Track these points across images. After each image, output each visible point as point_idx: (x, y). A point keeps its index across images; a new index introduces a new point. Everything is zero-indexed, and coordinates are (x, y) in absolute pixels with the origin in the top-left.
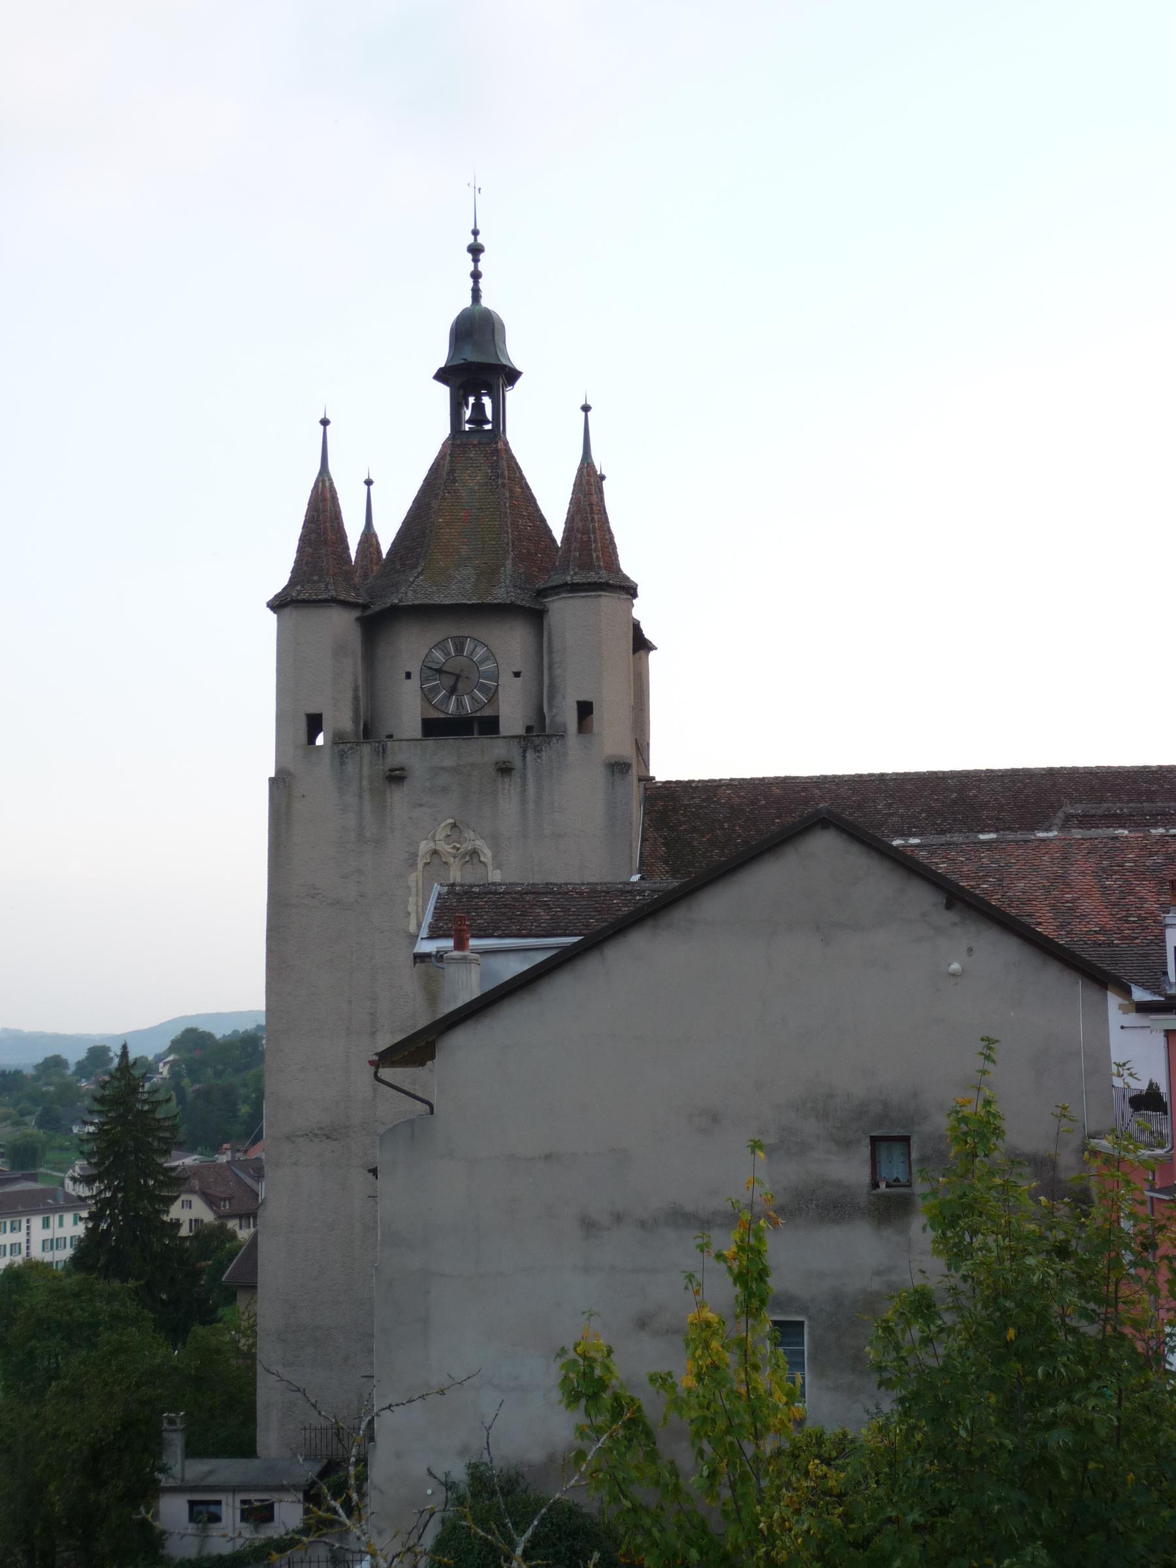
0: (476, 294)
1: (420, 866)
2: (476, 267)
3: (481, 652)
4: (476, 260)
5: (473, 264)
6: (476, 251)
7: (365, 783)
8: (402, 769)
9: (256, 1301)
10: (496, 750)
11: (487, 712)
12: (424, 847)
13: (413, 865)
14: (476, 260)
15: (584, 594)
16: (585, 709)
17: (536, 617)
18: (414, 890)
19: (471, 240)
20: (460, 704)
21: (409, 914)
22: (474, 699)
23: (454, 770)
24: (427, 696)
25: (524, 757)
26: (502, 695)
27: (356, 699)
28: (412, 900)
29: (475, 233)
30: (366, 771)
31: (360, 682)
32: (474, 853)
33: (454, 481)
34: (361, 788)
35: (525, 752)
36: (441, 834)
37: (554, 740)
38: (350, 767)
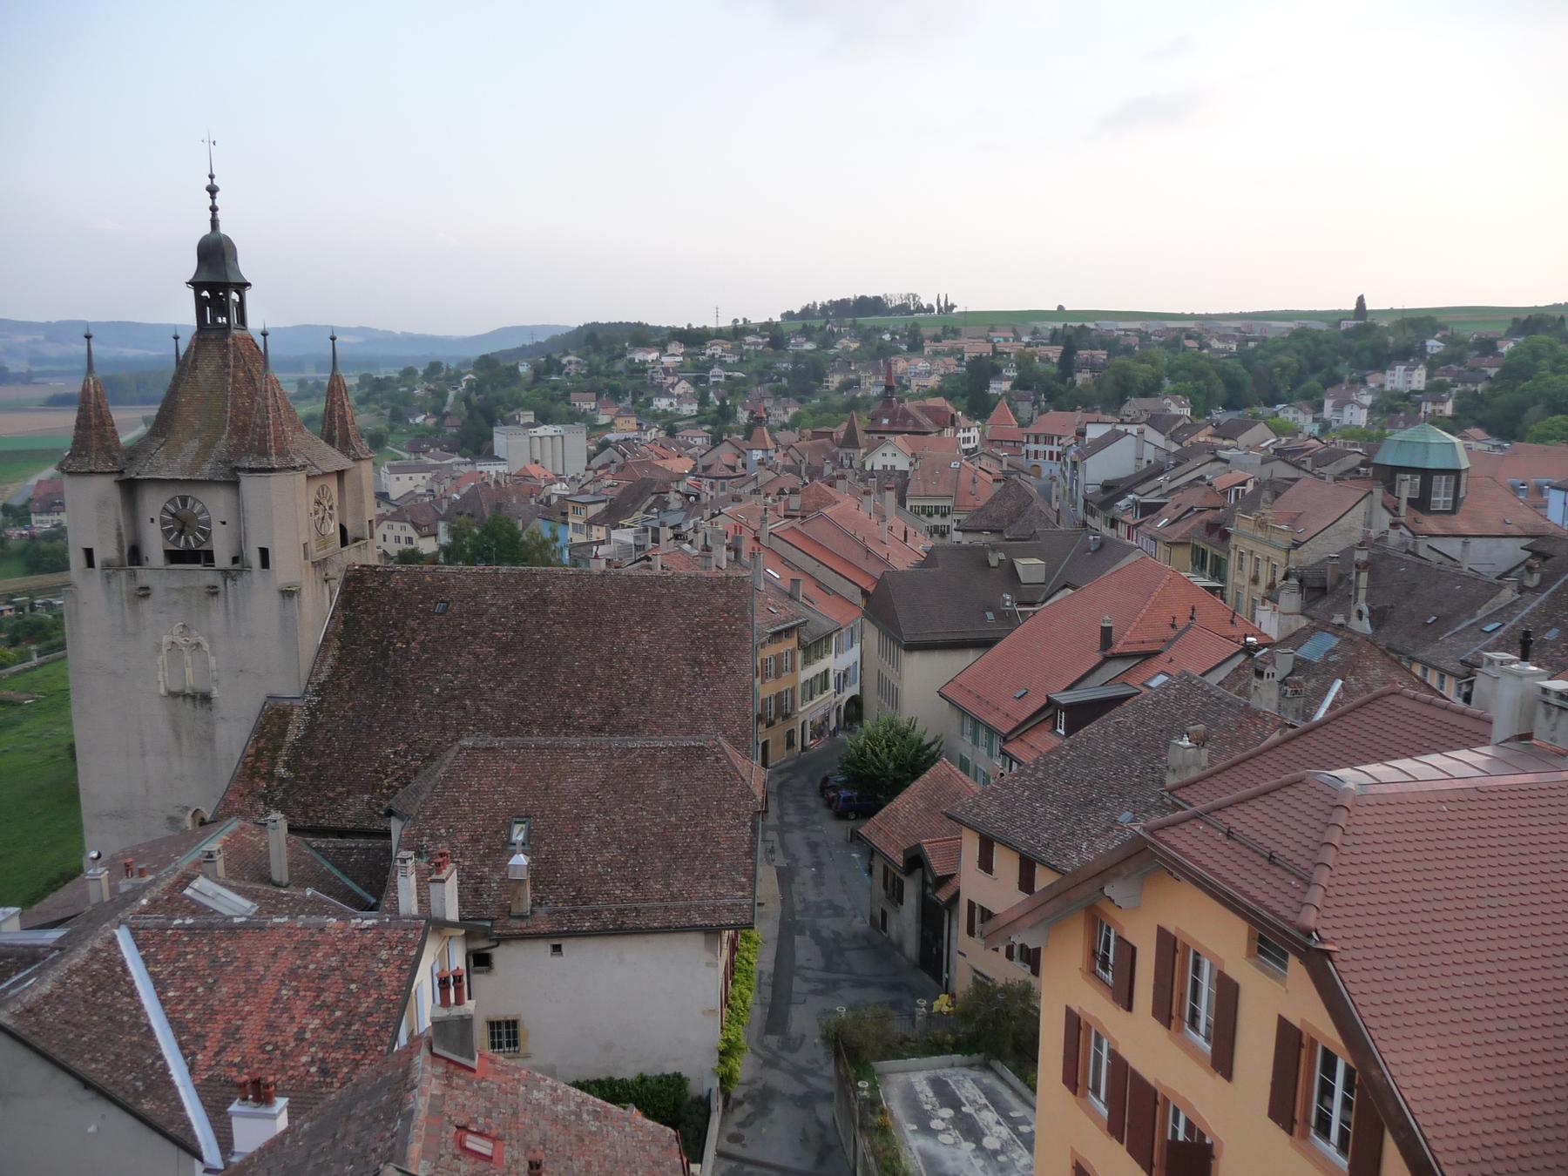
0: (214, 223)
1: (164, 651)
2: (213, 203)
3: (198, 508)
4: (213, 198)
6: (212, 191)
7: (124, 595)
8: (147, 588)
10: (208, 577)
11: (205, 547)
12: (166, 639)
13: (159, 651)
14: (213, 198)
16: (264, 553)
17: (235, 484)
18: (161, 667)
19: (208, 182)
20: (187, 541)
21: (159, 682)
22: (195, 538)
23: (181, 590)
24: (167, 533)
25: (225, 584)
26: (214, 536)
27: (119, 535)
28: (160, 673)
29: (212, 177)
30: (124, 588)
31: (122, 523)
32: (198, 644)
33: (196, 368)
35: (225, 580)
36: (177, 631)
37: (244, 573)
38: (114, 585)
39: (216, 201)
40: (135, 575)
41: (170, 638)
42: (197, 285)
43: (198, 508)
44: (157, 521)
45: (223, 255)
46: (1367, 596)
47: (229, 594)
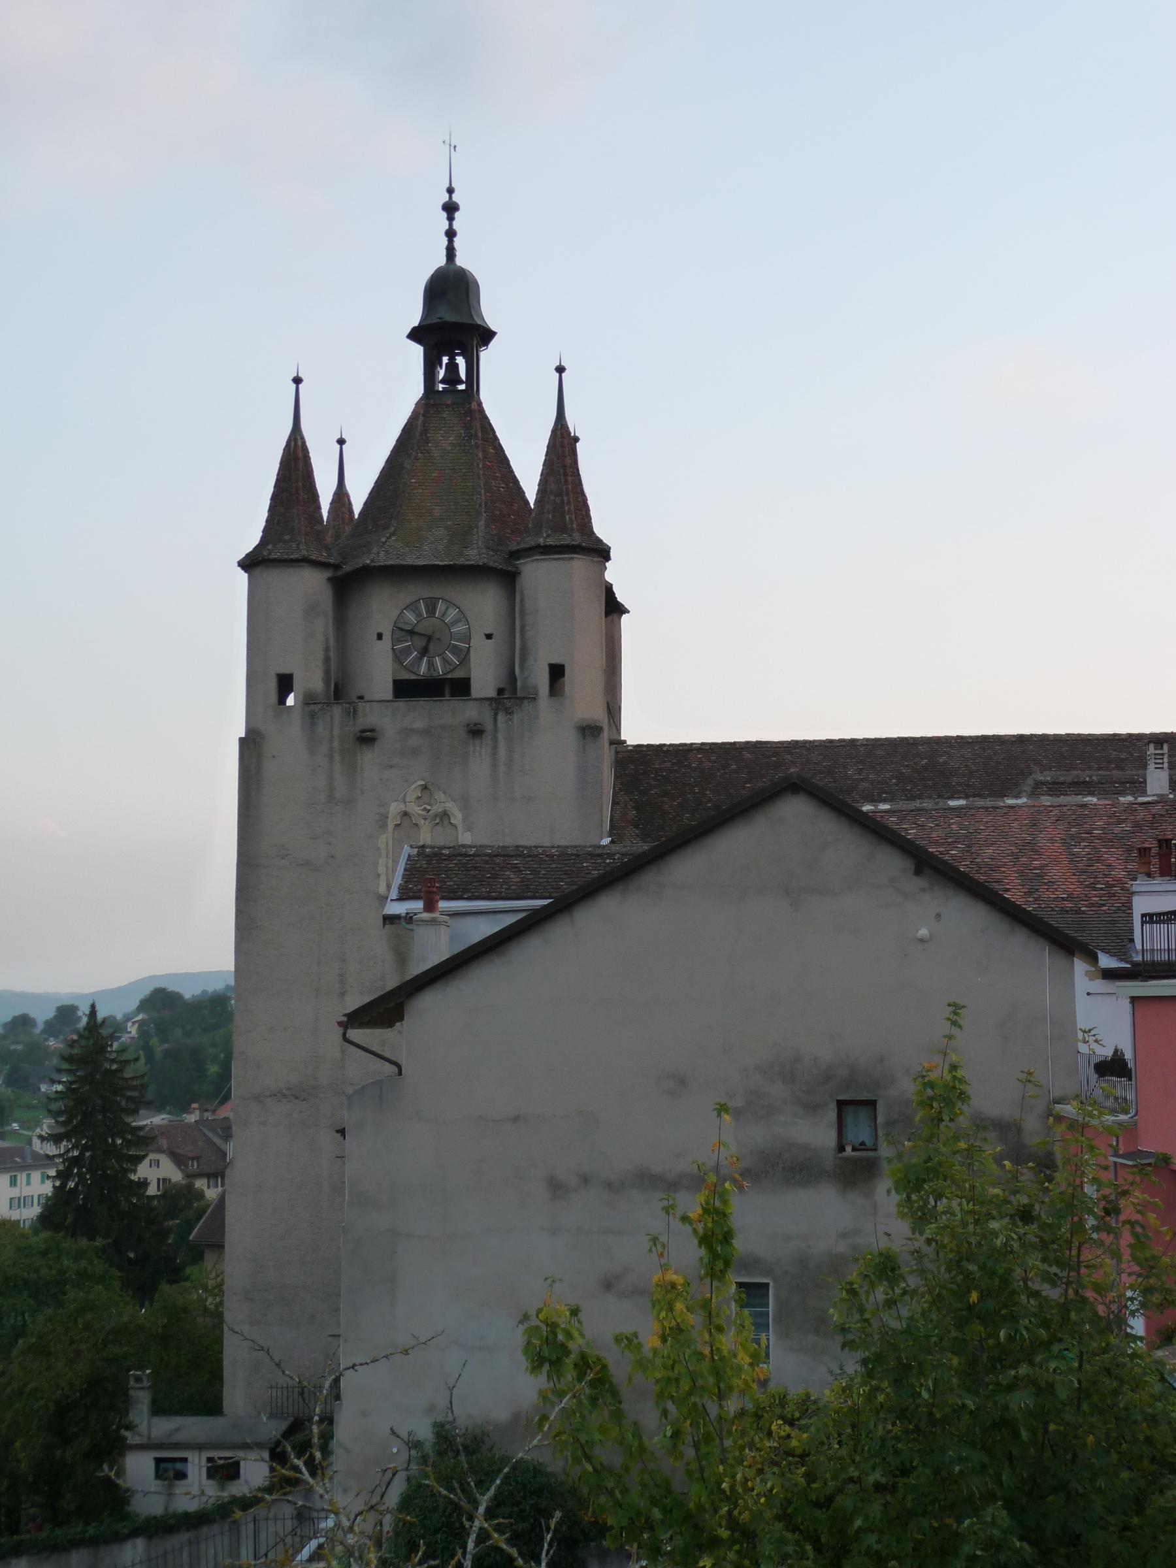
0: (451, 252)
1: (390, 827)
2: (451, 225)
4: (451, 219)
6: (450, 209)
7: (336, 744)
8: (373, 730)
10: (470, 712)
12: (395, 808)
14: (451, 219)
15: (556, 556)
16: (557, 672)
17: (509, 579)
18: (384, 852)
19: (446, 197)
20: (431, 665)
21: (379, 875)
22: (445, 661)
23: (426, 732)
24: (398, 657)
25: (495, 719)
27: (327, 660)
28: (382, 861)
29: (450, 191)
30: (336, 732)
33: (427, 441)
35: (496, 714)
37: (526, 702)
38: (321, 729)
39: (454, 223)
40: (355, 711)
41: (402, 807)
43: (452, 613)
44: (387, 637)
45: (467, 290)
47: (500, 736)
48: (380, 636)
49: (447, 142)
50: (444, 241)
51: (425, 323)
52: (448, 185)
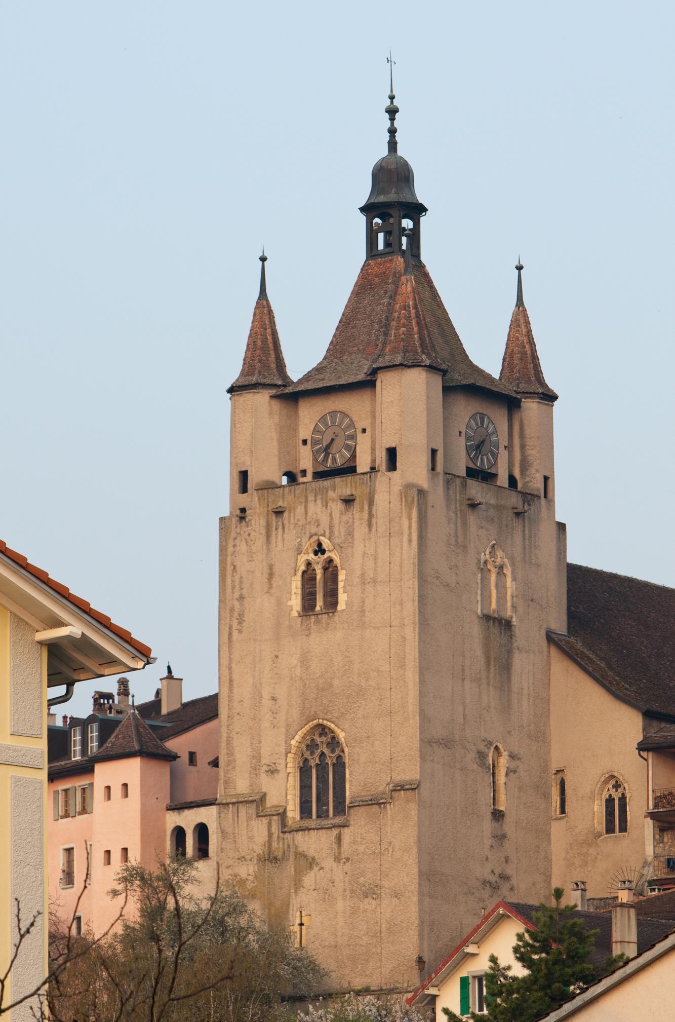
0: (393, 145)
2: (392, 124)
4: (392, 119)
5: (389, 122)
6: (392, 112)
9: (234, 768)
14: (392, 119)
15: (547, 402)
29: (392, 98)
34: (456, 508)
42: (416, 210)
44: (463, 434)
46: (337, 606)
48: (364, 431)
49: (393, 63)
50: (387, 136)
51: (372, 201)
52: (389, 93)
